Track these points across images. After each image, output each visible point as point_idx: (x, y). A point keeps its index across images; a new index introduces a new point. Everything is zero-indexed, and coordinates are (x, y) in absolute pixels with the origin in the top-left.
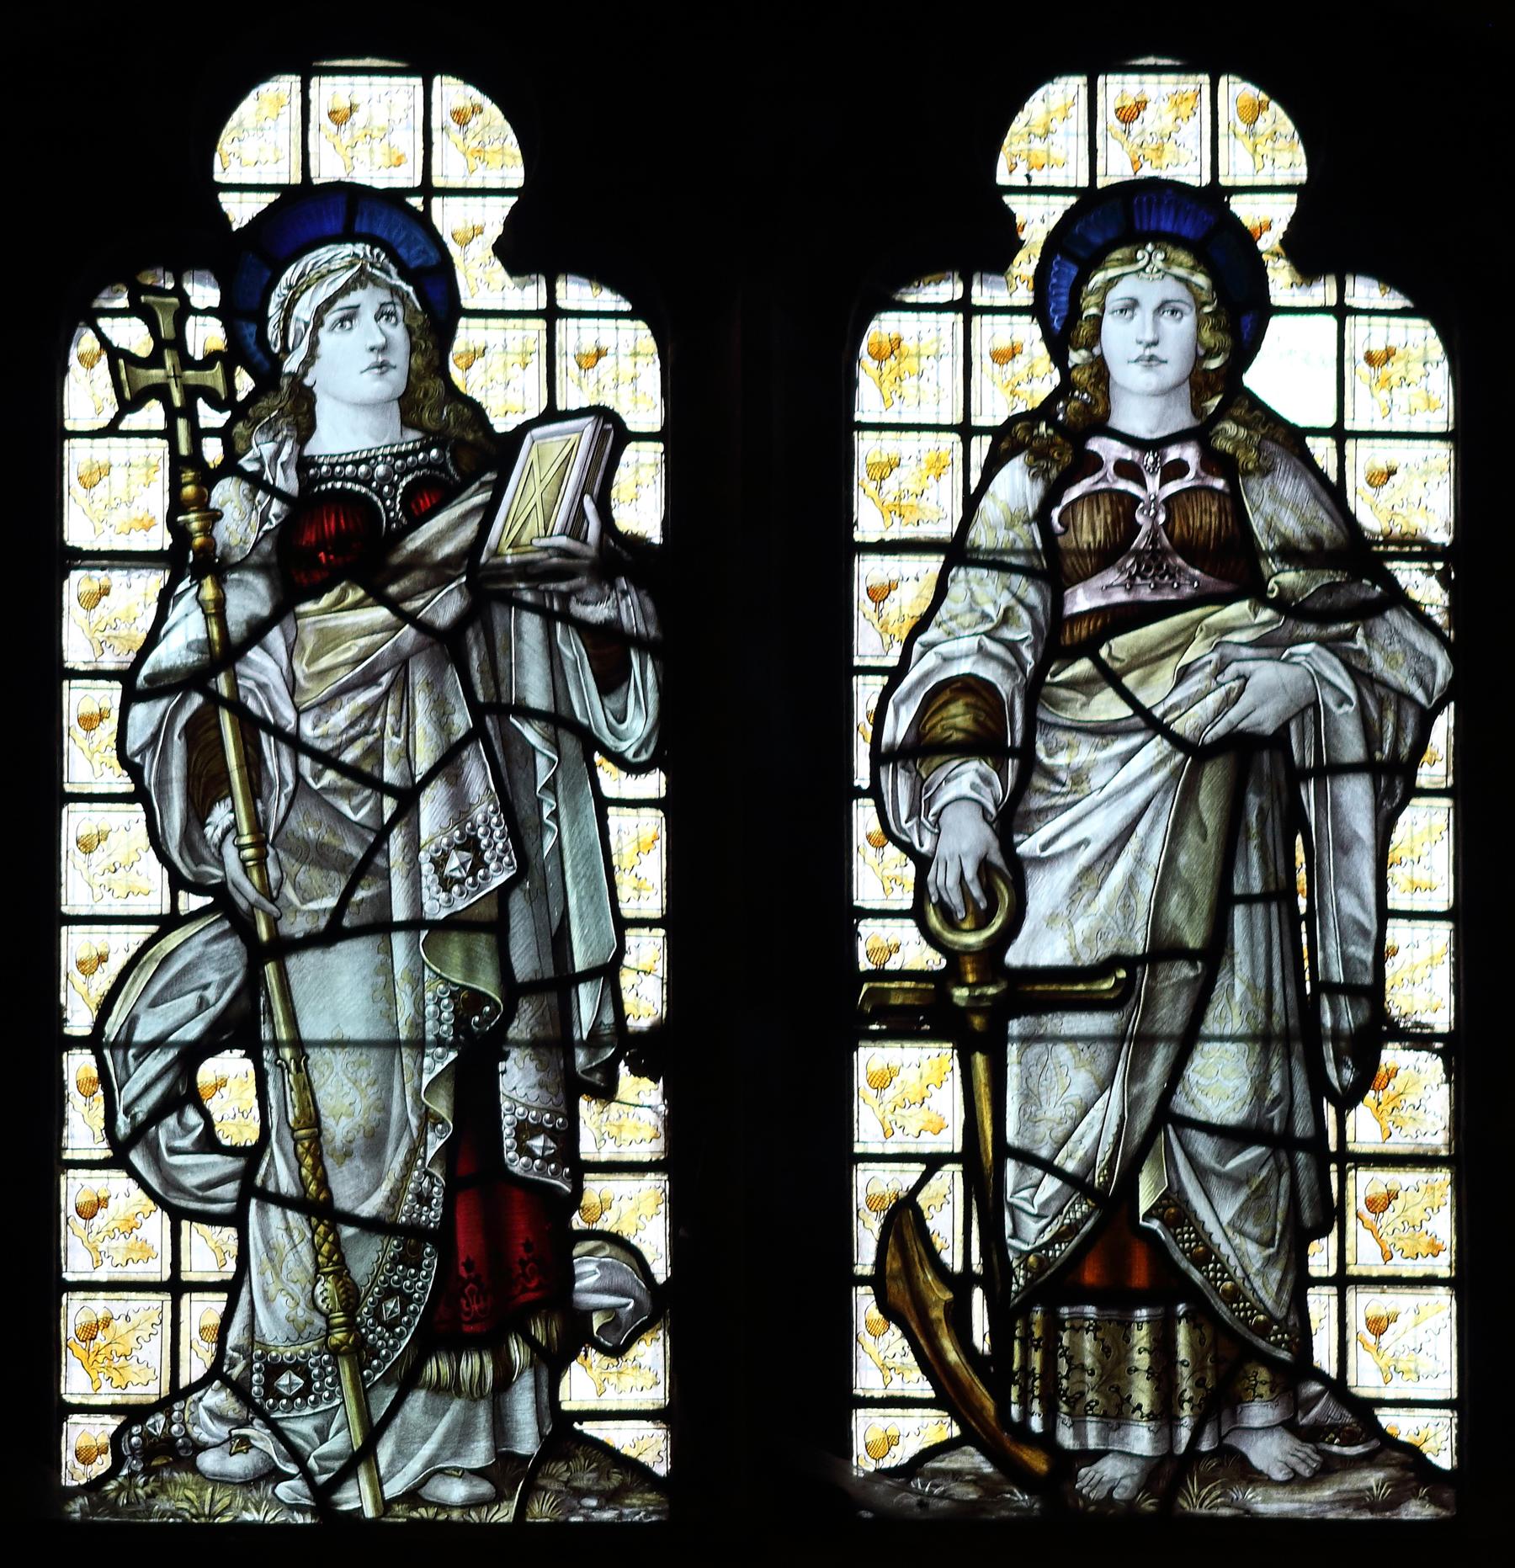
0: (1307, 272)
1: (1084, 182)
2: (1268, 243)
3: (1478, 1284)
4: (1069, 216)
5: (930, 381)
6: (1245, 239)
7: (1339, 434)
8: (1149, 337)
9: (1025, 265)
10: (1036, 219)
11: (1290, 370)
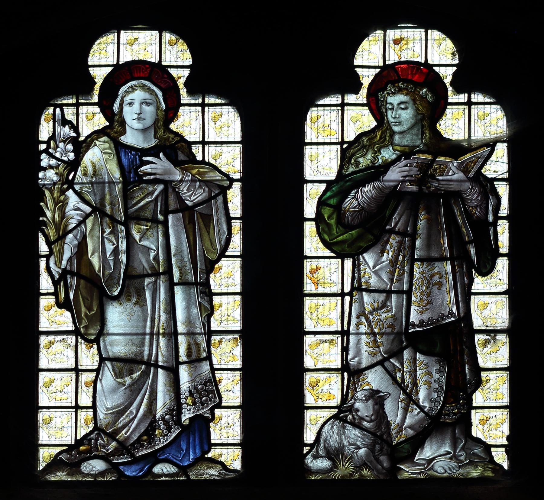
0: (191, 93)
1: (381, 64)
2: (181, 83)
3: (515, 407)
4: (377, 76)
5: (330, 129)
6: (173, 81)
7: (203, 143)
8: (138, 112)
9: (364, 92)
10: (367, 77)
11: (187, 124)
